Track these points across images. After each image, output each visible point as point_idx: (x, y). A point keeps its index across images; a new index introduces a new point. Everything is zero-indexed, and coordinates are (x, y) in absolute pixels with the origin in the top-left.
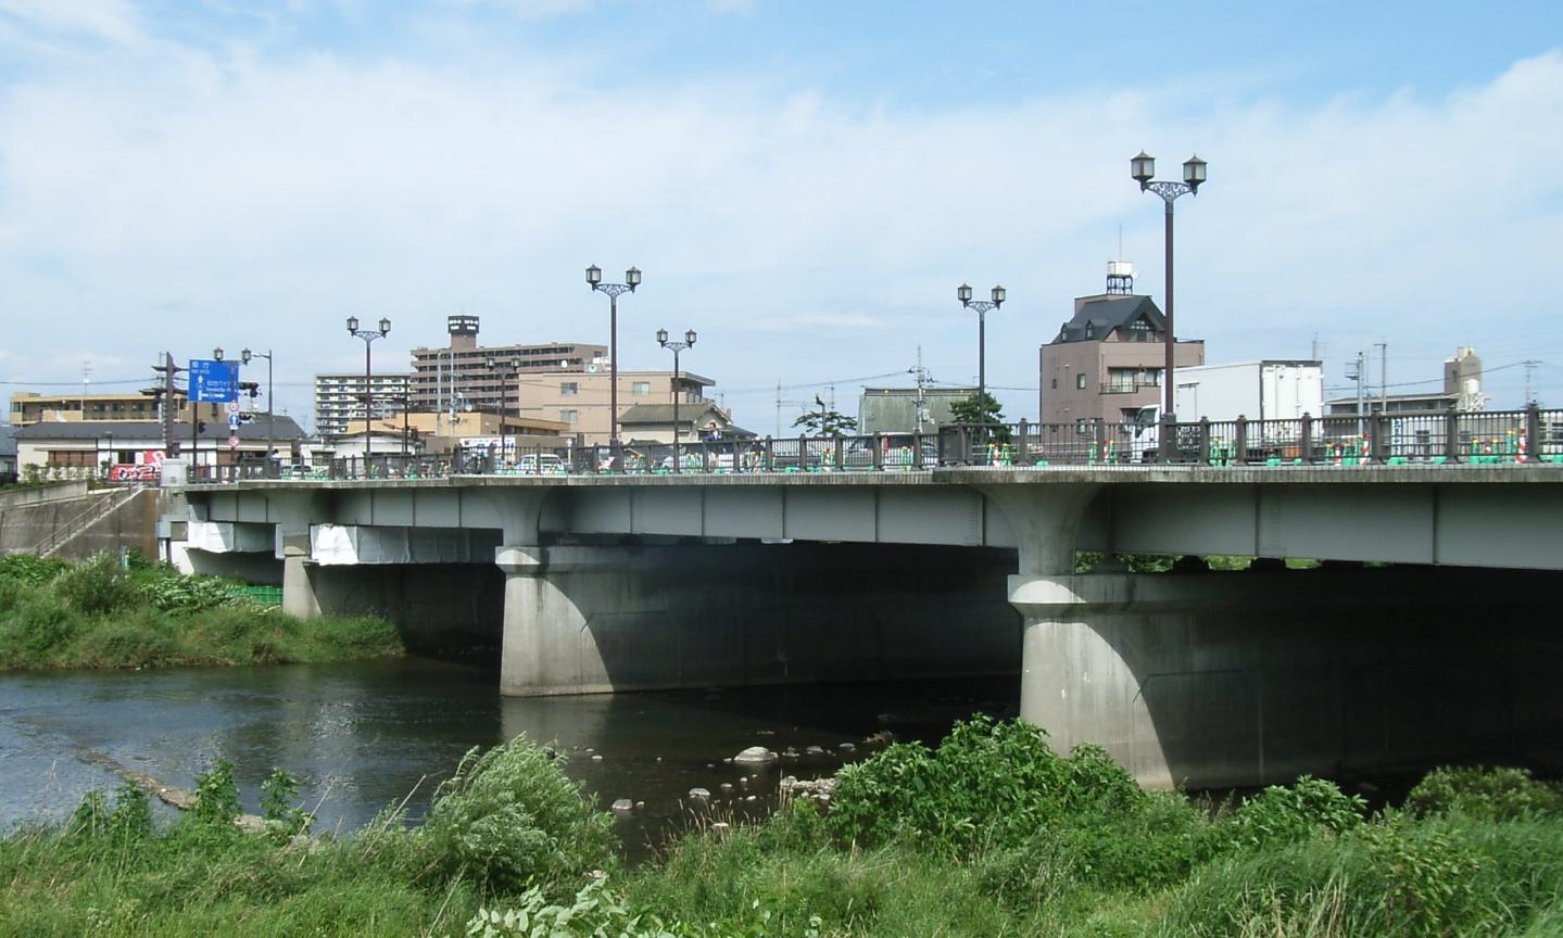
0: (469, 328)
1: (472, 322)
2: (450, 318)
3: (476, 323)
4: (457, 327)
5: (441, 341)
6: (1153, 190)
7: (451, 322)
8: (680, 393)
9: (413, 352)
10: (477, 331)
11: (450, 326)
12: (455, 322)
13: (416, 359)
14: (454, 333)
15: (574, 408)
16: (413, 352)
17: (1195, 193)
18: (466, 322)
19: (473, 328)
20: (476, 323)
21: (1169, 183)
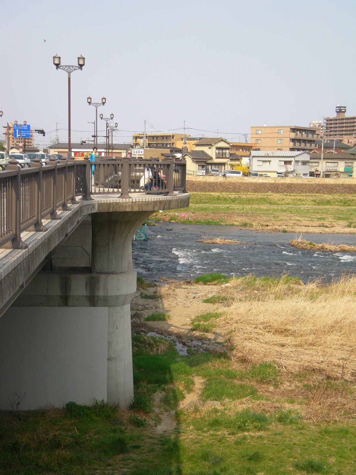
0: (342, 110)
1: (343, 108)
2: (337, 107)
3: (345, 109)
4: (338, 110)
5: (334, 115)
6: (62, 69)
7: (337, 109)
8: (72, 151)
9: (325, 119)
10: (345, 111)
11: (336, 110)
12: (338, 108)
13: (326, 121)
14: (337, 112)
15: (260, 139)
16: (325, 119)
17: (81, 70)
18: (341, 108)
19: (344, 110)
20: (345, 109)
21: (69, 66)
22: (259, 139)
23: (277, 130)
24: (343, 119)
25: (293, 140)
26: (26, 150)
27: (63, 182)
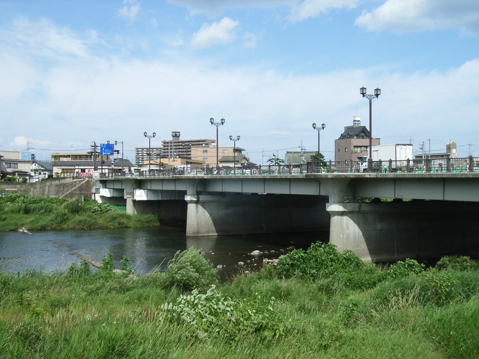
2: (172, 132)
5: (170, 138)
9: (162, 142)
10: (180, 136)
14: (173, 136)
16: (162, 142)
18: (177, 133)
22: (205, 157)
23: (222, 151)
24: (179, 142)
25: (136, 162)
26: (101, 170)
27: (314, 167)
